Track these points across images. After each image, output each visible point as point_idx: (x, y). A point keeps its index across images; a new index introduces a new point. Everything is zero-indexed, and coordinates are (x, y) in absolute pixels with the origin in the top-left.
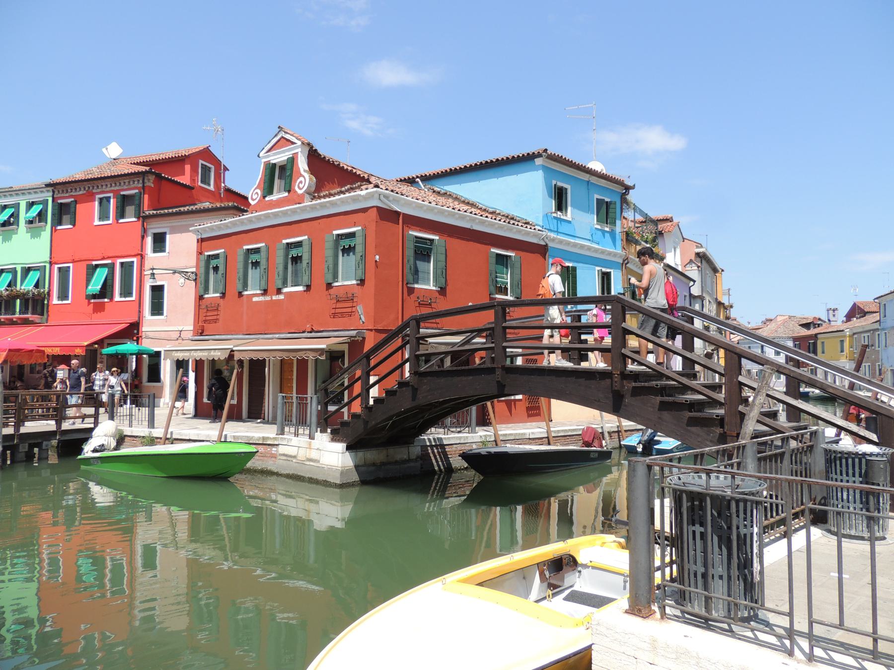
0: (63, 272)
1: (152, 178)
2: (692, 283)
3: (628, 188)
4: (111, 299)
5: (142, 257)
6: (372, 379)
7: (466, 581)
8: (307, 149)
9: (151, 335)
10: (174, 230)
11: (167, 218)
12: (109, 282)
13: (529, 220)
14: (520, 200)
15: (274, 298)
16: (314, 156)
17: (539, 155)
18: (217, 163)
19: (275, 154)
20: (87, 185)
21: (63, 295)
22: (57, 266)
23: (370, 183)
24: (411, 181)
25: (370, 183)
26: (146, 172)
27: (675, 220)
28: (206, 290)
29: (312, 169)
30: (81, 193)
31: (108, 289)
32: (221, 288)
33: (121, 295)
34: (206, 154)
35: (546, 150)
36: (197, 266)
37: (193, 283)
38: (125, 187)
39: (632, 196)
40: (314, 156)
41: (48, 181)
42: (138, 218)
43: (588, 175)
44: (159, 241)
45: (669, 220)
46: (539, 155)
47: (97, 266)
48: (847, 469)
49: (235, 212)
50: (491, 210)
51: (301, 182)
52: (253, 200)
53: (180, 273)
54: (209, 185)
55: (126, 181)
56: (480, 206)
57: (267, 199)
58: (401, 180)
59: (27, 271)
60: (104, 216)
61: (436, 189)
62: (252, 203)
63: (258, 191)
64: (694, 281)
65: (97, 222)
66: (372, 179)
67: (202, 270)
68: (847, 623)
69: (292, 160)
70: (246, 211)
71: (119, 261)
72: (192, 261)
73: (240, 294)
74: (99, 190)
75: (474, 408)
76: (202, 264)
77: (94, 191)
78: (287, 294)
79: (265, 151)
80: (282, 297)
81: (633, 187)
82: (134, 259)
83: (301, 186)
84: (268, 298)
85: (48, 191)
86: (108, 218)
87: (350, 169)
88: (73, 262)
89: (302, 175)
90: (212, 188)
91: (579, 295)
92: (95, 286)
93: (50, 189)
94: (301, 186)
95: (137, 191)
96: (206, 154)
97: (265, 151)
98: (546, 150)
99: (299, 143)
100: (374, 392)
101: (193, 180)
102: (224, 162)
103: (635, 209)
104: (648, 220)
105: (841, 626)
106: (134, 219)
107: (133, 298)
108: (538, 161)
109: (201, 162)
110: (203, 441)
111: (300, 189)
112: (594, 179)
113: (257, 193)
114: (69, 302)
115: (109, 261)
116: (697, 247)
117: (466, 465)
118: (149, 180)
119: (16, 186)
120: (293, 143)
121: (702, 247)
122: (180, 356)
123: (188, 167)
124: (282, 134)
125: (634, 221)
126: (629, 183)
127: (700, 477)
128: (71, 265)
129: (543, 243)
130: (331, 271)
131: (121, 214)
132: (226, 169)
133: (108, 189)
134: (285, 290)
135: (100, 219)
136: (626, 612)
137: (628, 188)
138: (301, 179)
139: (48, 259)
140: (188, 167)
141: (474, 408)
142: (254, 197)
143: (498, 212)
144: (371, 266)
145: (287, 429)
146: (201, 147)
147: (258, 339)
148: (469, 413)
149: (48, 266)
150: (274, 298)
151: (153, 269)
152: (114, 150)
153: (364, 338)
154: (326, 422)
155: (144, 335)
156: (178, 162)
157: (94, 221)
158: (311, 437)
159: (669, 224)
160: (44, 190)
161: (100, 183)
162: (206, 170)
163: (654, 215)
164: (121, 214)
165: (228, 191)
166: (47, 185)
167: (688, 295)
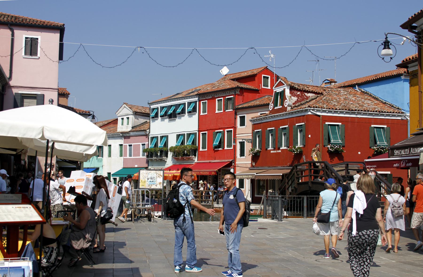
4: (223, 149)
5: (235, 128)
7: (131, 262)
9: (240, 165)
12: (222, 141)
15: (278, 151)
19: (278, 89)
22: (201, 133)
30: (210, 97)
31: (222, 144)
40: (292, 89)
47: (217, 132)
54: (268, 86)
57: (275, 108)
58: (340, 87)
59: (189, 135)
63: (272, 104)
65: (217, 112)
69: (284, 91)
71: (226, 130)
74: (217, 96)
77: (215, 97)
78: (282, 150)
80: (280, 151)
82: (232, 129)
84: (275, 152)
92: (216, 143)
115: (222, 130)
127: (397, 217)
131: (226, 107)
133: (221, 96)
138: (286, 100)
139: (197, 129)
147: (271, 169)
149: (197, 132)
157: (215, 111)
164: (226, 107)
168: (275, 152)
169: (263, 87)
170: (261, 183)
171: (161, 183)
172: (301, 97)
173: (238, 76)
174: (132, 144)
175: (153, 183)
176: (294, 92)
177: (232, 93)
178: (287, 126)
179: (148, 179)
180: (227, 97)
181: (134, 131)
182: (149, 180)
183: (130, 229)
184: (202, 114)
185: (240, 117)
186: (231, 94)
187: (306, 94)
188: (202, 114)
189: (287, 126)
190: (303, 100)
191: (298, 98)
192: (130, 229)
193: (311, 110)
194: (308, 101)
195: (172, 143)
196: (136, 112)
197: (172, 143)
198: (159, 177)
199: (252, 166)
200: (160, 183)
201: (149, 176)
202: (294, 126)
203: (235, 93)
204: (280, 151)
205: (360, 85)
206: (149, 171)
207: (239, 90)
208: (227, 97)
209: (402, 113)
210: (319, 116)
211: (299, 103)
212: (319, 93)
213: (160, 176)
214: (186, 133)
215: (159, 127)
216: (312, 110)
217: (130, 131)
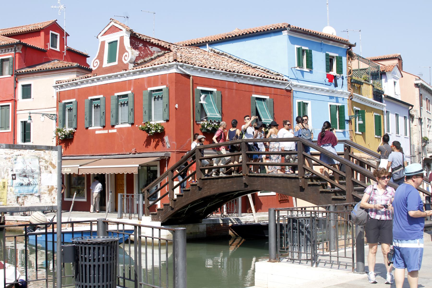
2: (410, 108)
3: (351, 46)
6: (176, 183)
13: (280, 73)
14: (275, 57)
15: (111, 131)
16: (135, 39)
17: (285, 29)
18: (61, 31)
23: (171, 51)
24: (200, 45)
28: (64, 125)
29: (133, 45)
32: (74, 125)
33: (9, 129)
34: (55, 26)
36: (57, 110)
37: (54, 121)
40: (135, 39)
42: (12, 75)
44: (27, 92)
51: (126, 56)
53: (47, 115)
54: (56, 47)
55: (4, 49)
56: (247, 63)
61: (216, 51)
63: (97, 61)
67: (61, 113)
68: (347, 256)
73: (87, 128)
75: (240, 199)
76: (61, 108)
78: (120, 129)
79: (101, 34)
80: (114, 131)
82: (10, 103)
83: (126, 58)
84: (106, 132)
89: (127, 52)
90: (58, 49)
94: (126, 58)
96: (55, 26)
97: (101, 34)
100: (177, 191)
102: (65, 31)
105: (345, 257)
108: (285, 33)
109: (51, 32)
111: (125, 60)
113: (97, 62)
116: (416, 80)
118: (18, 48)
120: (121, 30)
124: (112, 23)
126: (352, 43)
129: (290, 89)
132: (67, 35)
136: (89, 57)
138: (126, 54)
141: (240, 199)
142: (95, 65)
144: (173, 111)
145: (124, 215)
146: (51, 20)
148: (236, 202)
150: (111, 131)
153: (169, 158)
154: (150, 210)
165: (70, 51)
168: (106, 132)
169: (51, 48)
170: (73, 180)
171: (52, 188)
172: (143, 51)
173: (10, 32)
175: (31, 188)
176: (135, 43)
179: (14, 177)
182: (19, 180)
185: (23, 86)
187: (150, 47)
190: (146, 56)
191: (141, 53)
193: (179, 67)
194: (153, 57)
198: (46, 168)
200: (50, 190)
201: (19, 167)
202: (144, 92)
204: (114, 131)
205: (212, 43)
206: (16, 152)
207: (21, 47)
209: (286, 80)
210: (188, 76)
211: (142, 60)
212: (166, 49)
213: (50, 168)
216: (181, 66)
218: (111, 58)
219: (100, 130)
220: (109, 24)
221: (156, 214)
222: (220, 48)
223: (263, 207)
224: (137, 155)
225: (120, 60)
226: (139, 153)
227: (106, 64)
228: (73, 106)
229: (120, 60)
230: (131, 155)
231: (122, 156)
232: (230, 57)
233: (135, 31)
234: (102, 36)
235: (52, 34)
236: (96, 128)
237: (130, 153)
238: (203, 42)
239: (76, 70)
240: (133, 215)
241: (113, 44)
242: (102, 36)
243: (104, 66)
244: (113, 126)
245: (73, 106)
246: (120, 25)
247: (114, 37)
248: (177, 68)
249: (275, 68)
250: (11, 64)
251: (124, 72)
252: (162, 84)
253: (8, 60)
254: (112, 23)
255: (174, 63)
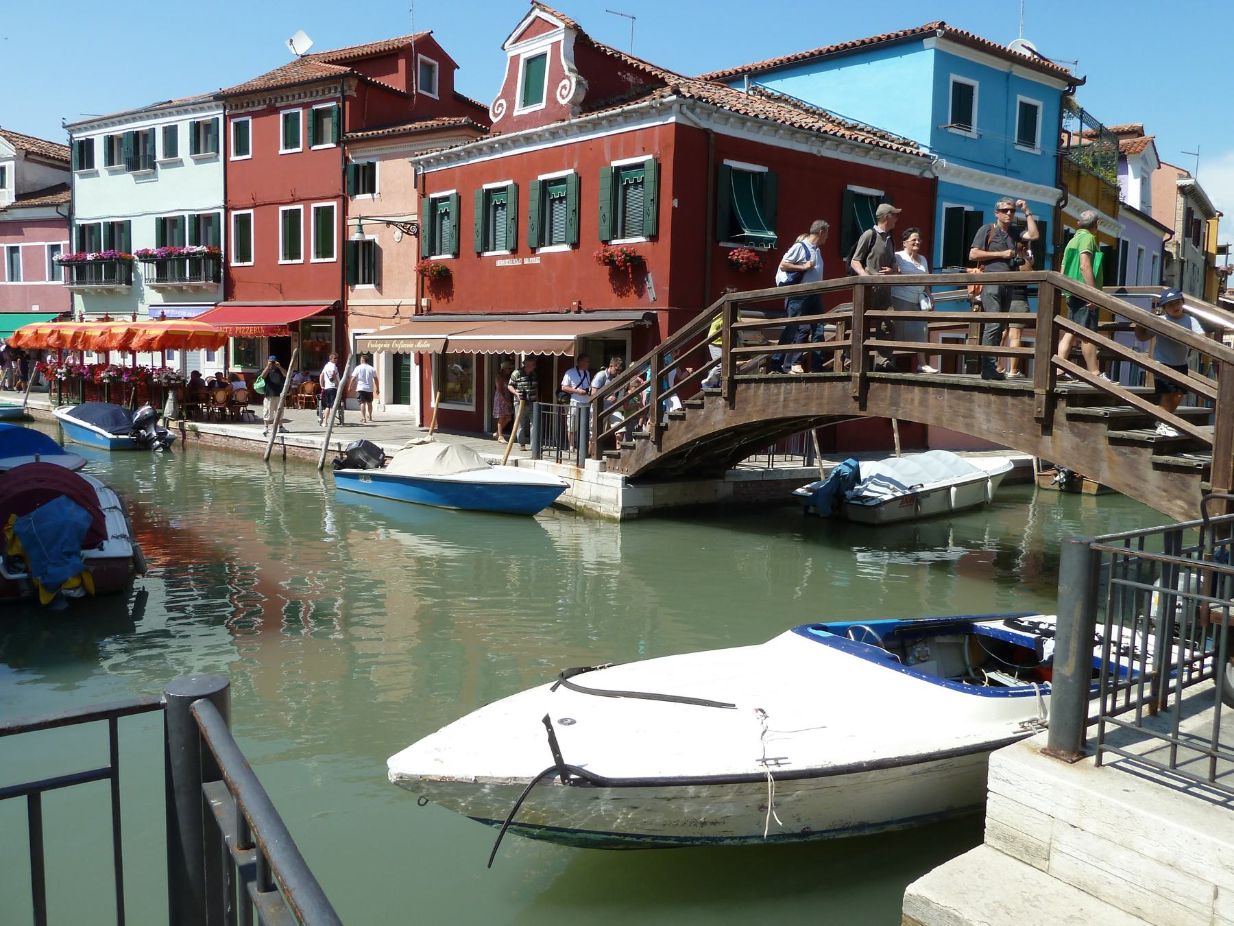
0: (243, 222)
1: (354, 83)
2: (1167, 236)
3: (1074, 83)
8: (573, 35)
9: (359, 311)
10: (384, 158)
11: (376, 143)
13: (910, 138)
15: (526, 262)
16: (587, 54)
17: (931, 33)
20: (267, 96)
21: (244, 255)
22: (233, 213)
25: (666, 85)
26: (345, 76)
27: (1148, 134)
30: (260, 108)
34: (427, 44)
35: (942, 25)
36: (419, 213)
38: (319, 98)
39: (1080, 97)
40: (587, 54)
41: (216, 90)
42: (338, 144)
43: (1007, 63)
45: (1139, 132)
46: (931, 33)
48: (458, 156)
49: (471, 133)
50: (851, 123)
51: (564, 87)
52: (496, 115)
56: (834, 116)
58: (712, 78)
60: (291, 141)
62: (495, 120)
63: (502, 101)
64: (1172, 233)
65: (282, 151)
66: (672, 81)
67: (427, 221)
70: (486, 132)
72: (412, 205)
73: (479, 254)
74: (284, 104)
76: (426, 211)
77: (278, 105)
80: (536, 260)
81: (1083, 82)
82: (334, 203)
83: (565, 92)
84: (517, 262)
85: (217, 106)
86: (297, 145)
87: (648, 69)
88: (254, 207)
91: (107, 721)
93: (220, 103)
94: (565, 92)
95: (334, 104)
98: (942, 25)
99: (562, 25)
101: (409, 85)
103: (1082, 115)
104: (1101, 133)
106: (333, 145)
107: (334, 259)
110: (358, 425)
112: (1019, 71)
114: (251, 264)
116: (1181, 177)
117: (1213, 710)
119: (176, 98)
121: (1189, 176)
122: (400, 347)
123: (402, 63)
125: (1081, 135)
126: (1076, 73)
128: (251, 211)
130: (608, 222)
133: (296, 102)
134: (543, 250)
135: (286, 146)
137: (1074, 83)
138: (566, 82)
140: (402, 63)
143: (861, 125)
149: (222, 212)
151: (360, 219)
152: (303, 45)
155: (350, 311)
156: (385, 58)
158: (580, 464)
159: (1138, 140)
160: (213, 104)
161: (284, 93)
162: (428, 68)
163: (1110, 125)
164: (317, 137)
166: (217, 97)
167: (1158, 254)
168: (517, 262)
174: (20, 245)
177: (332, 95)
178: (571, 171)
180: (315, 107)
181: (23, 207)
183: (732, 706)
184: (233, 158)
186: (328, 96)
188: (233, 158)
189: (571, 171)
192: (732, 706)
195: (144, 238)
196: (28, 153)
197: (144, 238)
199: (419, 310)
203: (343, 91)
204: (536, 260)
205: (758, 74)
208: (315, 107)
214: (186, 214)
215: (101, 196)
217: (8, 208)
218: (531, 96)
219: (504, 257)
220: (529, 15)
221: (618, 456)
222: (775, 86)
223: (67, 182)
224: (583, 315)
225: (552, 99)
226: (587, 312)
227: (519, 111)
228: (450, 206)
229: (552, 99)
230: (572, 315)
231: (551, 315)
232: (795, 106)
233: (586, 31)
234: (515, 42)
235: (423, 62)
236: (500, 255)
237: (568, 311)
238: (737, 72)
239: (464, 132)
240: (565, 454)
241: (535, 62)
242: (515, 42)
243: (516, 114)
244: (534, 250)
245: (450, 206)
246: (552, 14)
247: (539, 45)
248: (681, 112)
249: (898, 129)
250: (335, 120)
251: (559, 124)
252: (645, 151)
253: (329, 111)
254: (537, 12)
255: (674, 97)
